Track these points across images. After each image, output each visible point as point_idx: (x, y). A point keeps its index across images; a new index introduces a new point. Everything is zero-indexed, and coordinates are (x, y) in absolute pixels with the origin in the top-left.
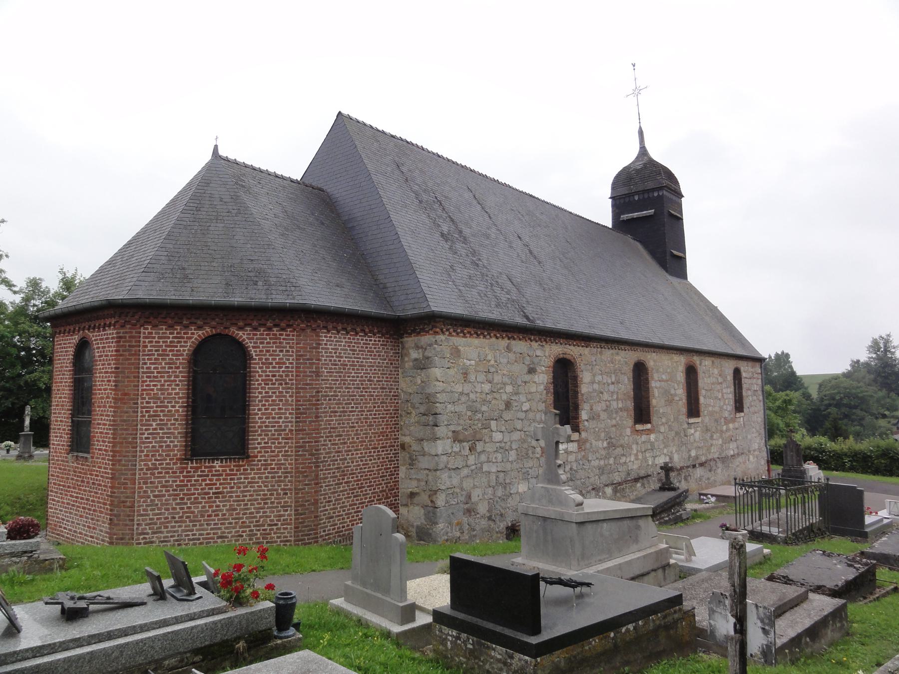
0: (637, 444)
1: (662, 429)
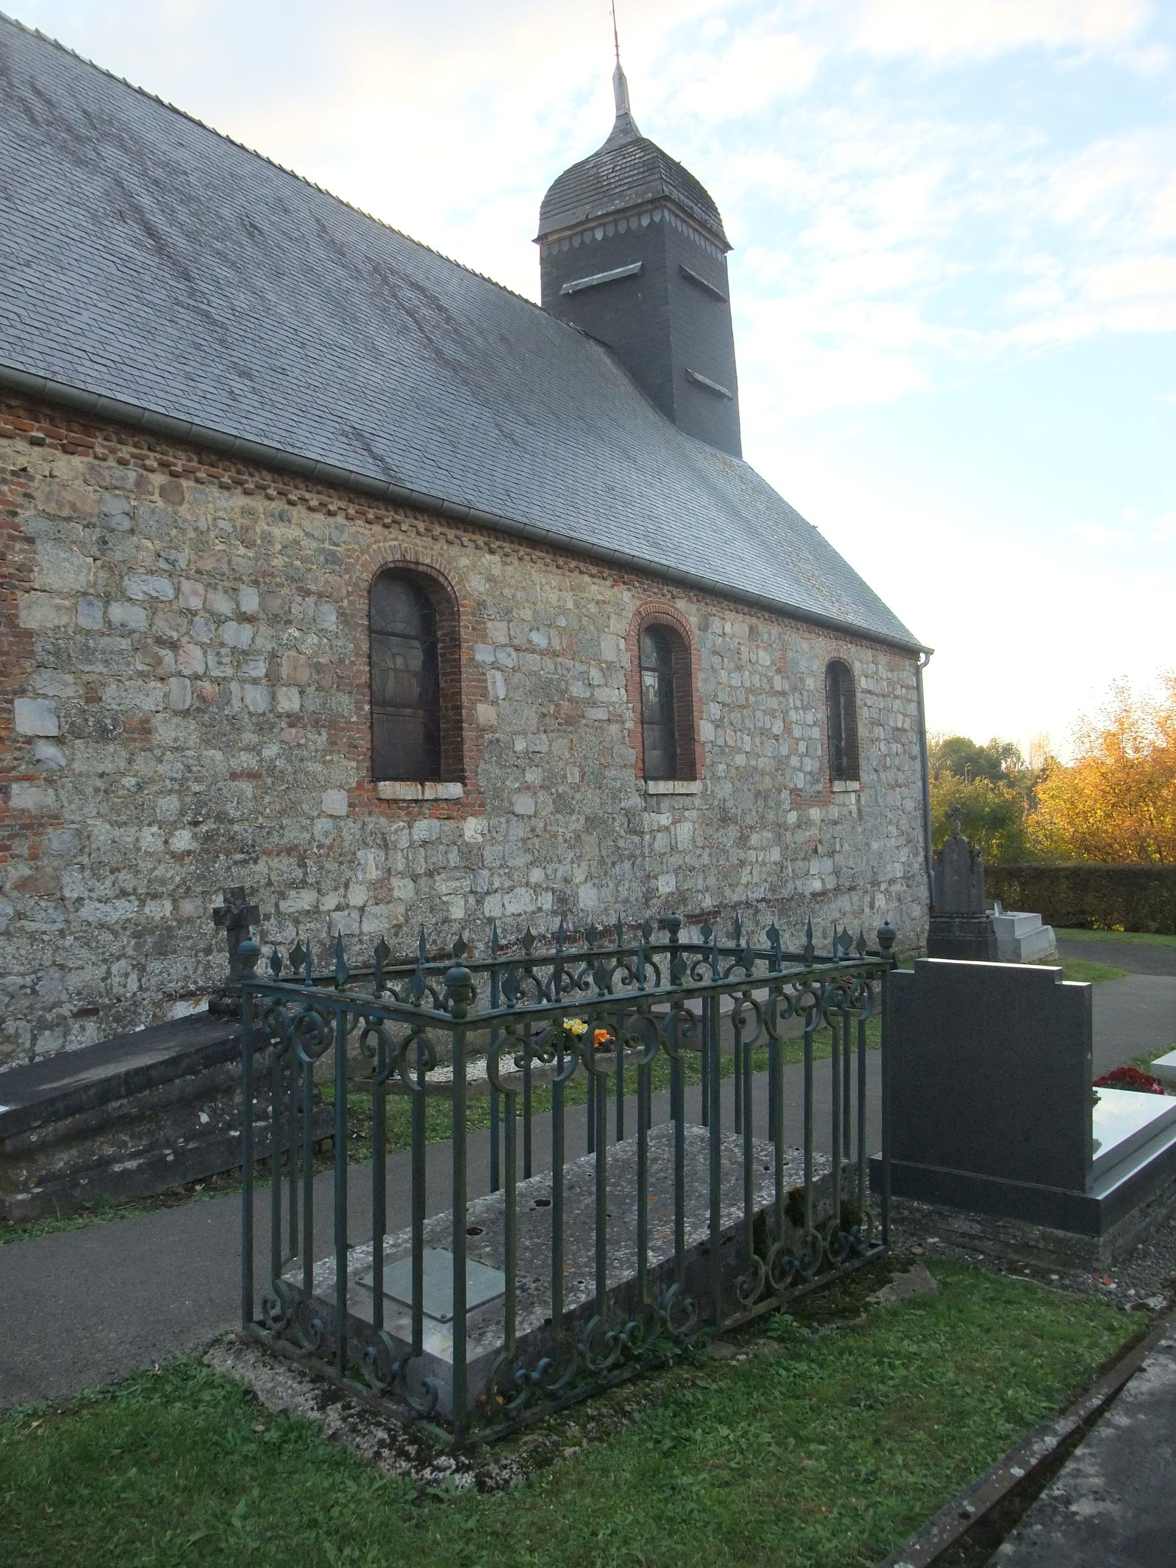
0: (385, 846)
1: (524, 804)
